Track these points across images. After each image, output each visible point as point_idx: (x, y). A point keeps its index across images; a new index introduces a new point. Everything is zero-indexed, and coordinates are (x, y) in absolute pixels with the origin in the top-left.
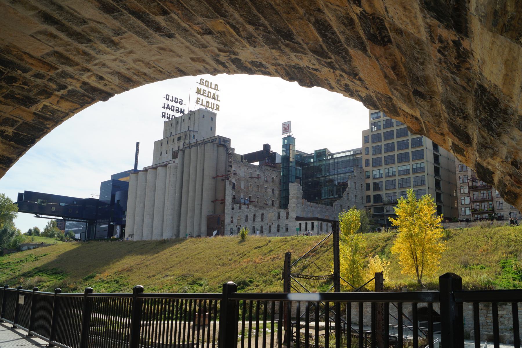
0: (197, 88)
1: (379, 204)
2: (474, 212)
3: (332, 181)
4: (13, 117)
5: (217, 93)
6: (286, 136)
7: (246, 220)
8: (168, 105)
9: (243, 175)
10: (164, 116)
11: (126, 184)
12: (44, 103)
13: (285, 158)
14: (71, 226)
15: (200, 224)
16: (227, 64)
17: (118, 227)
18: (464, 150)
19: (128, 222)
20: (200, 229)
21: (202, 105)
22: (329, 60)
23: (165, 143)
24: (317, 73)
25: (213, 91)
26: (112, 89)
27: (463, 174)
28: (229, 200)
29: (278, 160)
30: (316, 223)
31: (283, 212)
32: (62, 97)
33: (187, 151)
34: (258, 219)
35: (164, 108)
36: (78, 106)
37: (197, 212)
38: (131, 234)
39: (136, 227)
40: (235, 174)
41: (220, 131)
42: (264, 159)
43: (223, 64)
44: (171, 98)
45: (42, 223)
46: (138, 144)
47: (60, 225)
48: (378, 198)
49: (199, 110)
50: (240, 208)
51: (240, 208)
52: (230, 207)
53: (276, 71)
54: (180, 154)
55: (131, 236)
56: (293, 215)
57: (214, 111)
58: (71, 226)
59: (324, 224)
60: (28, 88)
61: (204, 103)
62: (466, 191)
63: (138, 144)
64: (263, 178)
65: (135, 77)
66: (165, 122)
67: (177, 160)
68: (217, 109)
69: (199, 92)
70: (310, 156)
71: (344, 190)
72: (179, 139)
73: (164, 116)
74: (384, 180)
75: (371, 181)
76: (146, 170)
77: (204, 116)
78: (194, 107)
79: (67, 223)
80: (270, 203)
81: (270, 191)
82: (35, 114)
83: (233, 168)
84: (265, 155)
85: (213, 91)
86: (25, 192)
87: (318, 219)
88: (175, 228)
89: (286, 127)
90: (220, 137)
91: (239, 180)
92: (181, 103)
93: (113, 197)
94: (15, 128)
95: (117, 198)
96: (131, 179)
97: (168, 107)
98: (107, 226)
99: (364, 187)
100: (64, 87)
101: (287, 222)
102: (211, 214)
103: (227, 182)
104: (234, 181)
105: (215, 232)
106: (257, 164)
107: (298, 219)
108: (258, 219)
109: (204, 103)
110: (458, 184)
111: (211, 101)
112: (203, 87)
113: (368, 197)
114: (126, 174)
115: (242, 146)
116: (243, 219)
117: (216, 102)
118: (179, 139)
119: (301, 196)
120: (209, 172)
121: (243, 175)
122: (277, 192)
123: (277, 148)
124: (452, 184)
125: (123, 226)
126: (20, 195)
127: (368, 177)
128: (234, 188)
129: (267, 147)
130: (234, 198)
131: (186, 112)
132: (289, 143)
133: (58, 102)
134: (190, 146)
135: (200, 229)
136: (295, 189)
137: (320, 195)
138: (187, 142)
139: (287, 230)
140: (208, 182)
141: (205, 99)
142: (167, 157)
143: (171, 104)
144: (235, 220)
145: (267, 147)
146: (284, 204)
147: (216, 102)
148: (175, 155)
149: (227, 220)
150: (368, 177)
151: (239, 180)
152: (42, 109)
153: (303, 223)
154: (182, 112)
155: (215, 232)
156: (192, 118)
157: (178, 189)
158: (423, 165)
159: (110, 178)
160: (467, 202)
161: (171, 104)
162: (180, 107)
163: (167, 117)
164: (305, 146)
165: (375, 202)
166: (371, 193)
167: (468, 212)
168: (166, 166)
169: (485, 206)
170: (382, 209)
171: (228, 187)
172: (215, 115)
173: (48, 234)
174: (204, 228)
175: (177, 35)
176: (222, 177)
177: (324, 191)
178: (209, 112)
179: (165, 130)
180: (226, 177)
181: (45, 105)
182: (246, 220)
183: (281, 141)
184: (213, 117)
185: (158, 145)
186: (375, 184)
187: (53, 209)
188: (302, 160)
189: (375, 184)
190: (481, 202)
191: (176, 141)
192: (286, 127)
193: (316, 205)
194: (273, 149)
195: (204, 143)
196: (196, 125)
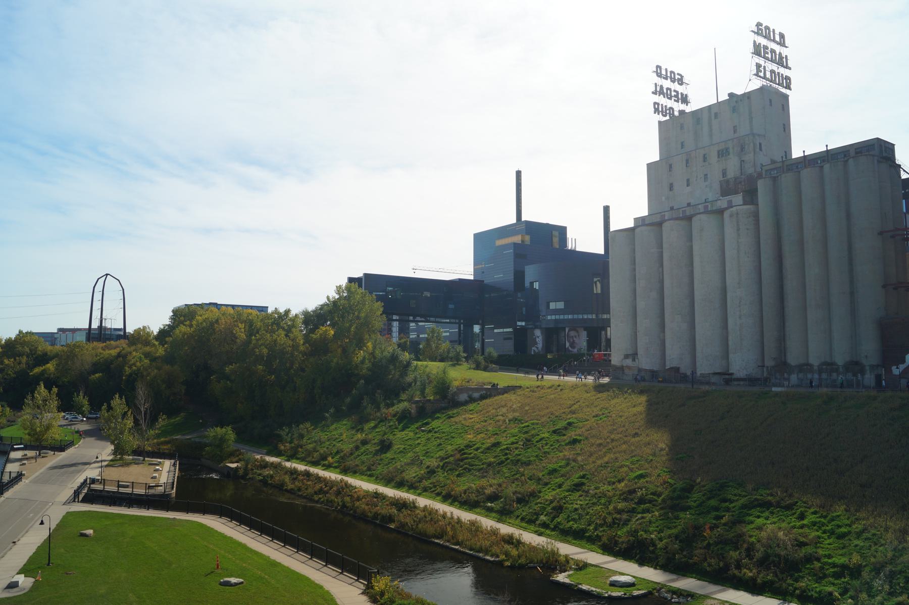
0: (755, 42)
5: (785, 52)
8: (661, 87)
10: (656, 111)
21: (764, 78)
35: (655, 93)
38: (630, 352)
44: (664, 72)
46: (519, 174)
49: (762, 89)
57: (784, 90)
61: (768, 75)
66: (660, 122)
68: (788, 87)
69: (758, 50)
77: (771, 101)
86: (365, 275)
92: (681, 82)
93: (519, 276)
98: (510, 330)
143: (667, 84)
161: (667, 84)
163: (662, 111)
172: (786, 97)
191: (713, 157)
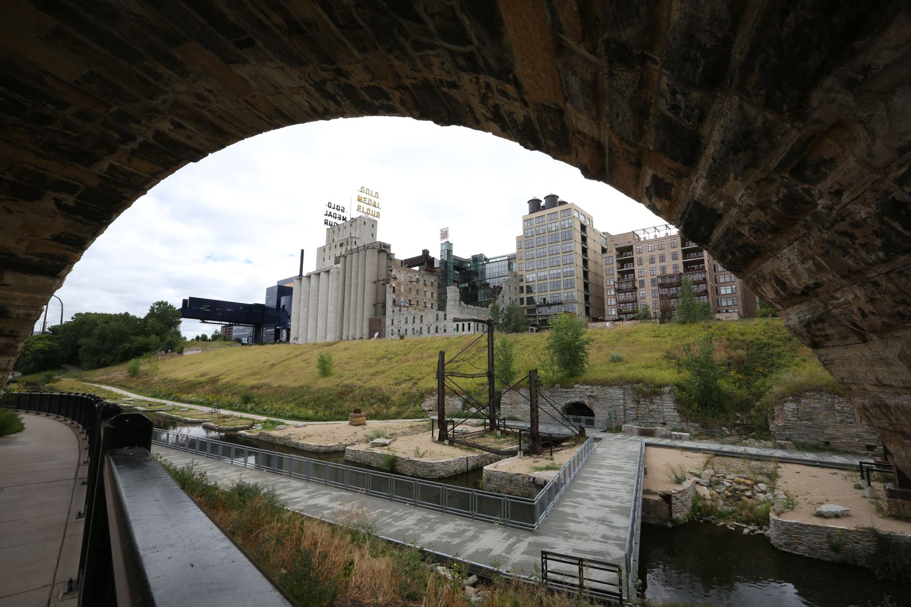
1: (532, 306)
2: (620, 312)
3: (488, 284)
4: (67, 180)
5: (377, 201)
6: (444, 241)
7: (406, 322)
9: (402, 279)
10: (326, 223)
11: (291, 289)
12: (110, 161)
13: (444, 263)
14: (239, 331)
15: (362, 327)
16: (339, 98)
17: (284, 331)
18: (672, 186)
19: (293, 324)
20: (362, 331)
22: (468, 49)
23: (327, 249)
24: (453, 92)
25: (373, 199)
26: (201, 144)
27: (610, 277)
28: (389, 303)
29: (436, 265)
30: (472, 324)
31: (441, 313)
32: (134, 152)
33: (348, 257)
34: (418, 321)
36: (162, 169)
37: (359, 315)
39: (301, 330)
40: (395, 278)
41: (382, 237)
42: (423, 264)
43: (333, 98)
45: (210, 329)
46: (302, 251)
47: (227, 330)
48: (531, 300)
50: (400, 311)
51: (400, 311)
52: (391, 310)
53: (403, 103)
54: (342, 259)
55: (296, 339)
56: (450, 317)
57: (375, 218)
58: (239, 331)
59: (480, 325)
60: (77, 135)
61: (365, 211)
62: (613, 293)
63: (302, 251)
64: (422, 282)
65: (226, 127)
67: (339, 266)
69: (359, 200)
70: (467, 261)
71: (499, 292)
72: (341, 245)
73: (326, 223)
74: (536, 283)
75: (524, 284)
76: (309, 277)
78: (356, 215)
79: (235, 328)
80: (429, 305)
81: (429, 294)
82: (100, 176)
83: (394, 273)
84: (425, 260)
85: (373, 199)
87: (475, 321)
88: (338, 331)
89: (444, 234)
90: (381, 244)
91: (399, 284)
93: (279, 302)
94: (76, 195)
95: (282, 304)
96: (295, 285)
97: (330, 215)
99: (518, 290)
100: (130, 138)
101: (446, 323)
102: (372, 316)
103: (388, 286)
104: (394, 285)
105: (376, 334)
106: (417, 268)
107: (455, 320)
108: (418, 321)
109: (365, 211)
110: (605, 286)
111: (372, 208)
112: (363, 195)
113: (522, 299)
114: (290, 280)
115: (402, 252)
116: (404, 321)
117: (377, 210)
118: (341, 245)
119: (458, 298)
120: (370, 275)
121: (402, 279)
122: (435, 295)
123: (436, 254)
124: (600, 288)
125: (289, 330)
126: (185, 301)
127: (522, 280)
128: (394, 291)
129: (426, 252)
130: (394, 301)
131: (348, 219)
132: (448, 249)
133: (129, 160)
134: (351, 252)
135: (362, 331)
136: (453, 292)
137: (476, 299)
138: (349, 248)
139: (445, 331)
140: (369, 286)
141: (366, 207)
142: (330, 263)
143: (333, 211)
144: (395, 322)
145: (426, 252)
146: (442, 306)
147: (377, 210)
148: (337, 262)
149: (388, 322)
150: (522, 280)
151: (399, 284)
152: (109, 169)
153: (460, 324)
154: (344, 219)
155: (376, 334)
156: (354, 224)
157: (340, 294)
158: (572, 269)
159: (275, 284)
160: (613, 303)
161: (333, 211)
162: (342, 214)
164: (463, 252)
165: (528, 303)
166: (525, 295)
167: (614, 313)
168: (328, 272)
169: (629, 307)
170: (534, 310)
171: (389, 290)
172: (376, 222)
173: (215, 337)
174: (366, 331)
175: (259, 43)
176: (382, 282)
177: (481, 293)
178: (369, 219)
179: (328, 237)
180: (387, 281)
181: (111, 165)
182: (406, 322)
183: (440, 246)
184: (374, 225)
185: (322, 250)
186: (528, 287)
187: (220, 314)
188: (460, 265)
189: (528, 287)
190: (625, 303)
192: (444, 234)
193: (472, 307)
194: (431, 254)
195: (366, 248)
196: (358, 231)
